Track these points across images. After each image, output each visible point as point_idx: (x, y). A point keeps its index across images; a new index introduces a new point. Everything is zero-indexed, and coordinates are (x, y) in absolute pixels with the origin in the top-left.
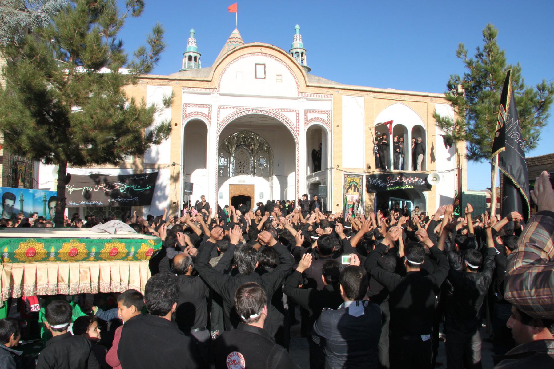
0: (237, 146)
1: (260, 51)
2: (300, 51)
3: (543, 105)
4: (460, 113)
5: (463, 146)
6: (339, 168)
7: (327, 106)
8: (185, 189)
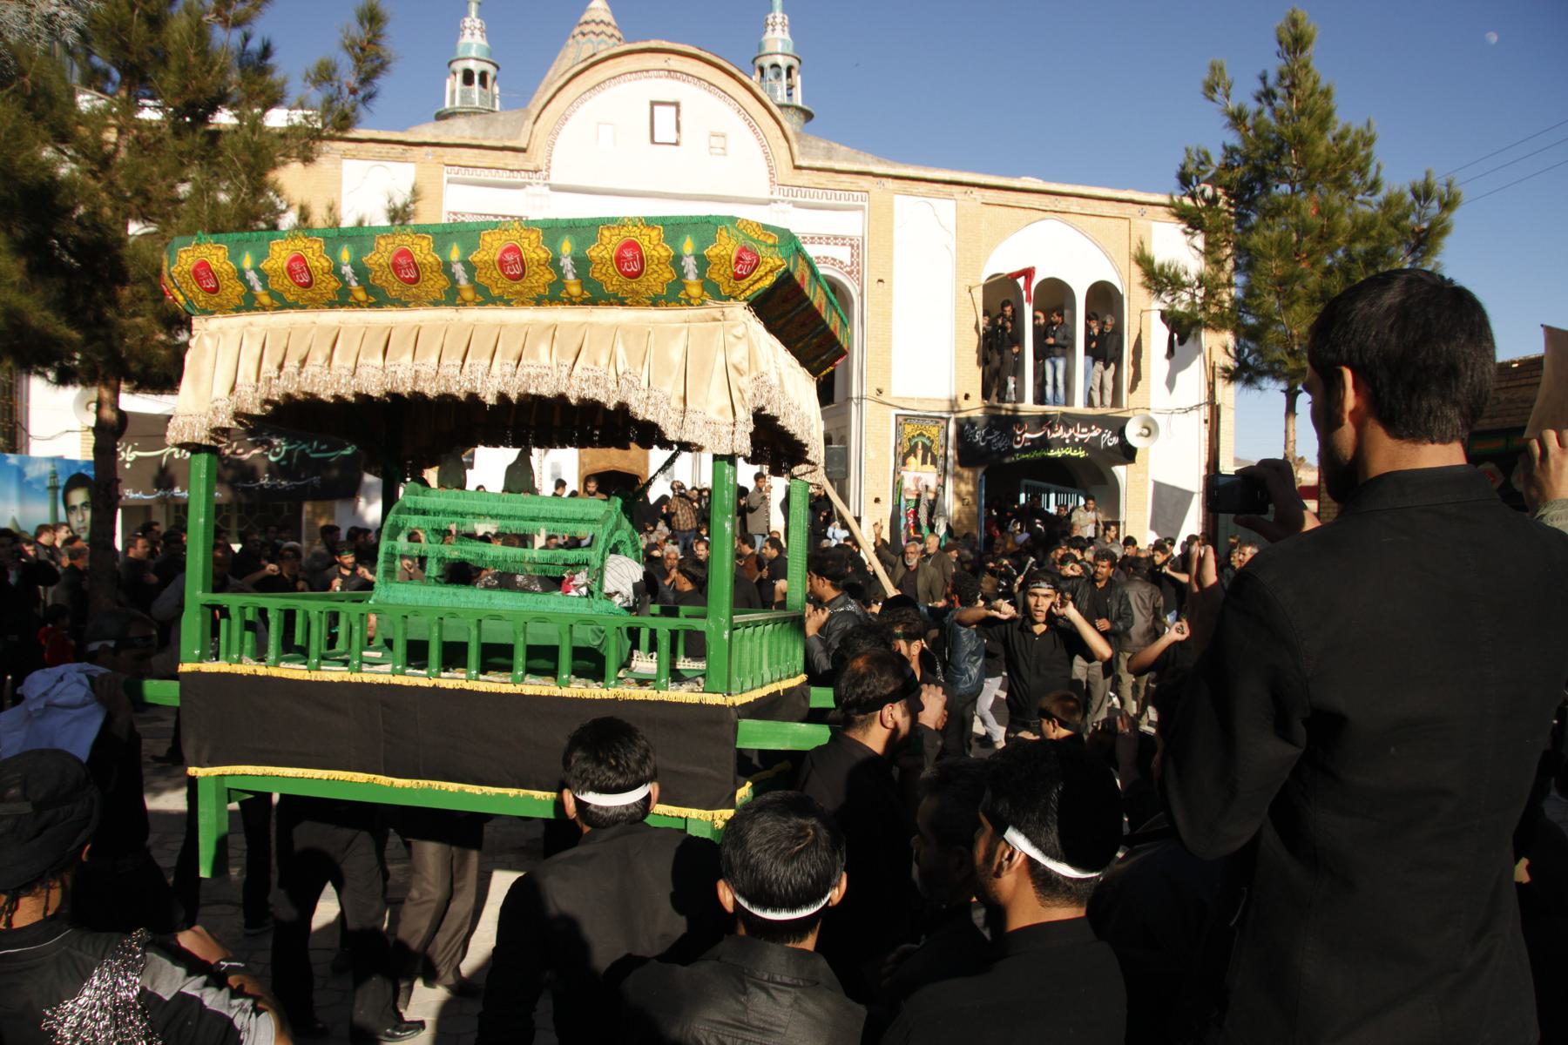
1: (665, 66)
2: (783, 61)
3: (1426, 238)
4: (1210, 252)
5: (1217, 345)
6: (882, 398)
7: (850, 224)
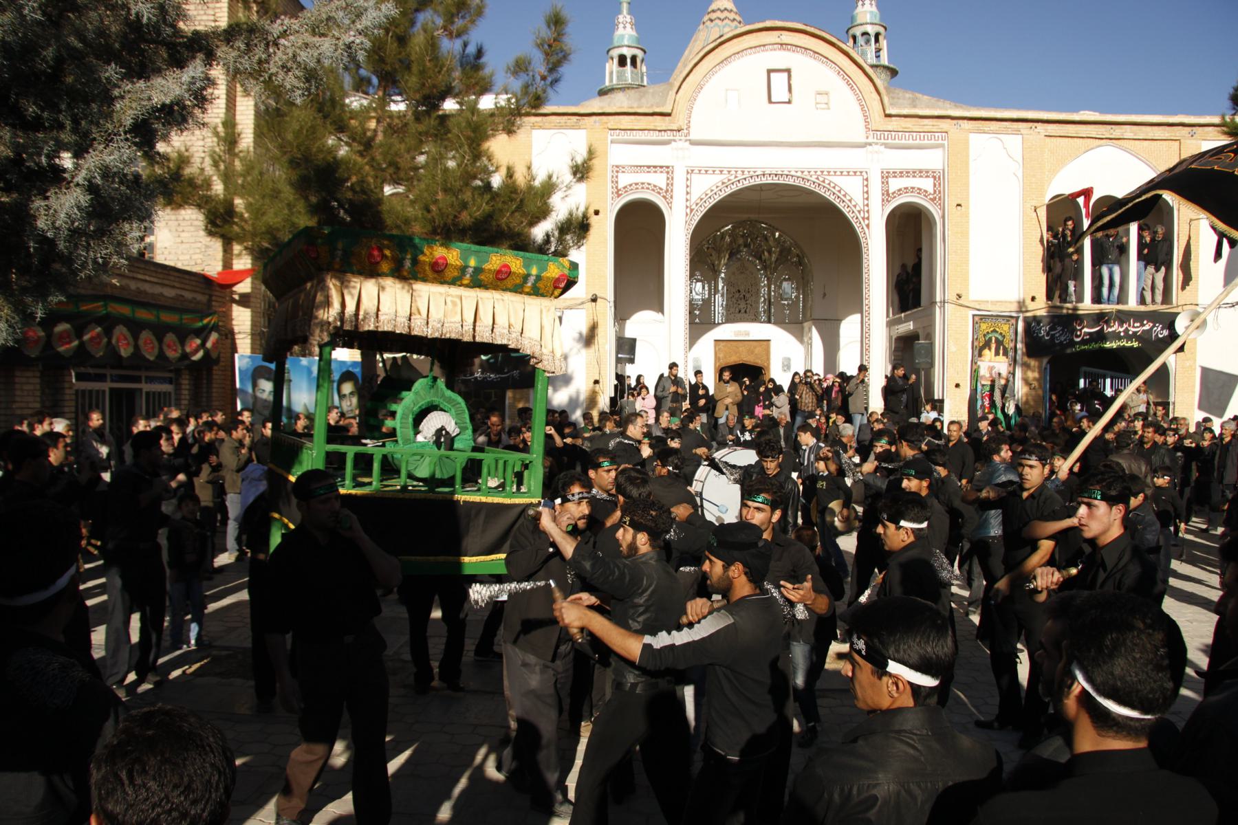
0: (731, 255)
1: (778, 40)
2: (871, 30)
6: (960, 302)
7: (932, 159)
8: (617, 353)
